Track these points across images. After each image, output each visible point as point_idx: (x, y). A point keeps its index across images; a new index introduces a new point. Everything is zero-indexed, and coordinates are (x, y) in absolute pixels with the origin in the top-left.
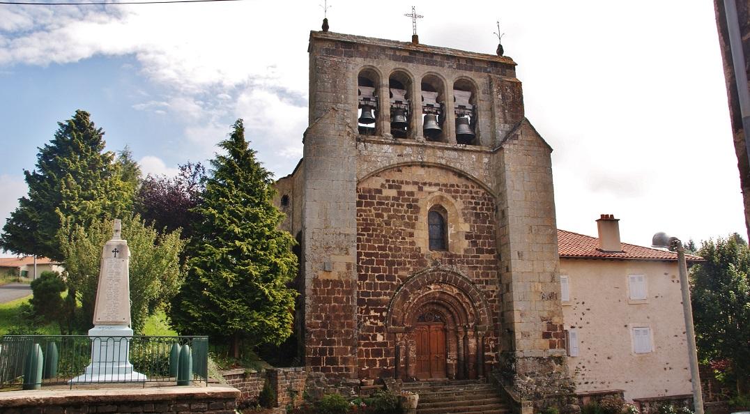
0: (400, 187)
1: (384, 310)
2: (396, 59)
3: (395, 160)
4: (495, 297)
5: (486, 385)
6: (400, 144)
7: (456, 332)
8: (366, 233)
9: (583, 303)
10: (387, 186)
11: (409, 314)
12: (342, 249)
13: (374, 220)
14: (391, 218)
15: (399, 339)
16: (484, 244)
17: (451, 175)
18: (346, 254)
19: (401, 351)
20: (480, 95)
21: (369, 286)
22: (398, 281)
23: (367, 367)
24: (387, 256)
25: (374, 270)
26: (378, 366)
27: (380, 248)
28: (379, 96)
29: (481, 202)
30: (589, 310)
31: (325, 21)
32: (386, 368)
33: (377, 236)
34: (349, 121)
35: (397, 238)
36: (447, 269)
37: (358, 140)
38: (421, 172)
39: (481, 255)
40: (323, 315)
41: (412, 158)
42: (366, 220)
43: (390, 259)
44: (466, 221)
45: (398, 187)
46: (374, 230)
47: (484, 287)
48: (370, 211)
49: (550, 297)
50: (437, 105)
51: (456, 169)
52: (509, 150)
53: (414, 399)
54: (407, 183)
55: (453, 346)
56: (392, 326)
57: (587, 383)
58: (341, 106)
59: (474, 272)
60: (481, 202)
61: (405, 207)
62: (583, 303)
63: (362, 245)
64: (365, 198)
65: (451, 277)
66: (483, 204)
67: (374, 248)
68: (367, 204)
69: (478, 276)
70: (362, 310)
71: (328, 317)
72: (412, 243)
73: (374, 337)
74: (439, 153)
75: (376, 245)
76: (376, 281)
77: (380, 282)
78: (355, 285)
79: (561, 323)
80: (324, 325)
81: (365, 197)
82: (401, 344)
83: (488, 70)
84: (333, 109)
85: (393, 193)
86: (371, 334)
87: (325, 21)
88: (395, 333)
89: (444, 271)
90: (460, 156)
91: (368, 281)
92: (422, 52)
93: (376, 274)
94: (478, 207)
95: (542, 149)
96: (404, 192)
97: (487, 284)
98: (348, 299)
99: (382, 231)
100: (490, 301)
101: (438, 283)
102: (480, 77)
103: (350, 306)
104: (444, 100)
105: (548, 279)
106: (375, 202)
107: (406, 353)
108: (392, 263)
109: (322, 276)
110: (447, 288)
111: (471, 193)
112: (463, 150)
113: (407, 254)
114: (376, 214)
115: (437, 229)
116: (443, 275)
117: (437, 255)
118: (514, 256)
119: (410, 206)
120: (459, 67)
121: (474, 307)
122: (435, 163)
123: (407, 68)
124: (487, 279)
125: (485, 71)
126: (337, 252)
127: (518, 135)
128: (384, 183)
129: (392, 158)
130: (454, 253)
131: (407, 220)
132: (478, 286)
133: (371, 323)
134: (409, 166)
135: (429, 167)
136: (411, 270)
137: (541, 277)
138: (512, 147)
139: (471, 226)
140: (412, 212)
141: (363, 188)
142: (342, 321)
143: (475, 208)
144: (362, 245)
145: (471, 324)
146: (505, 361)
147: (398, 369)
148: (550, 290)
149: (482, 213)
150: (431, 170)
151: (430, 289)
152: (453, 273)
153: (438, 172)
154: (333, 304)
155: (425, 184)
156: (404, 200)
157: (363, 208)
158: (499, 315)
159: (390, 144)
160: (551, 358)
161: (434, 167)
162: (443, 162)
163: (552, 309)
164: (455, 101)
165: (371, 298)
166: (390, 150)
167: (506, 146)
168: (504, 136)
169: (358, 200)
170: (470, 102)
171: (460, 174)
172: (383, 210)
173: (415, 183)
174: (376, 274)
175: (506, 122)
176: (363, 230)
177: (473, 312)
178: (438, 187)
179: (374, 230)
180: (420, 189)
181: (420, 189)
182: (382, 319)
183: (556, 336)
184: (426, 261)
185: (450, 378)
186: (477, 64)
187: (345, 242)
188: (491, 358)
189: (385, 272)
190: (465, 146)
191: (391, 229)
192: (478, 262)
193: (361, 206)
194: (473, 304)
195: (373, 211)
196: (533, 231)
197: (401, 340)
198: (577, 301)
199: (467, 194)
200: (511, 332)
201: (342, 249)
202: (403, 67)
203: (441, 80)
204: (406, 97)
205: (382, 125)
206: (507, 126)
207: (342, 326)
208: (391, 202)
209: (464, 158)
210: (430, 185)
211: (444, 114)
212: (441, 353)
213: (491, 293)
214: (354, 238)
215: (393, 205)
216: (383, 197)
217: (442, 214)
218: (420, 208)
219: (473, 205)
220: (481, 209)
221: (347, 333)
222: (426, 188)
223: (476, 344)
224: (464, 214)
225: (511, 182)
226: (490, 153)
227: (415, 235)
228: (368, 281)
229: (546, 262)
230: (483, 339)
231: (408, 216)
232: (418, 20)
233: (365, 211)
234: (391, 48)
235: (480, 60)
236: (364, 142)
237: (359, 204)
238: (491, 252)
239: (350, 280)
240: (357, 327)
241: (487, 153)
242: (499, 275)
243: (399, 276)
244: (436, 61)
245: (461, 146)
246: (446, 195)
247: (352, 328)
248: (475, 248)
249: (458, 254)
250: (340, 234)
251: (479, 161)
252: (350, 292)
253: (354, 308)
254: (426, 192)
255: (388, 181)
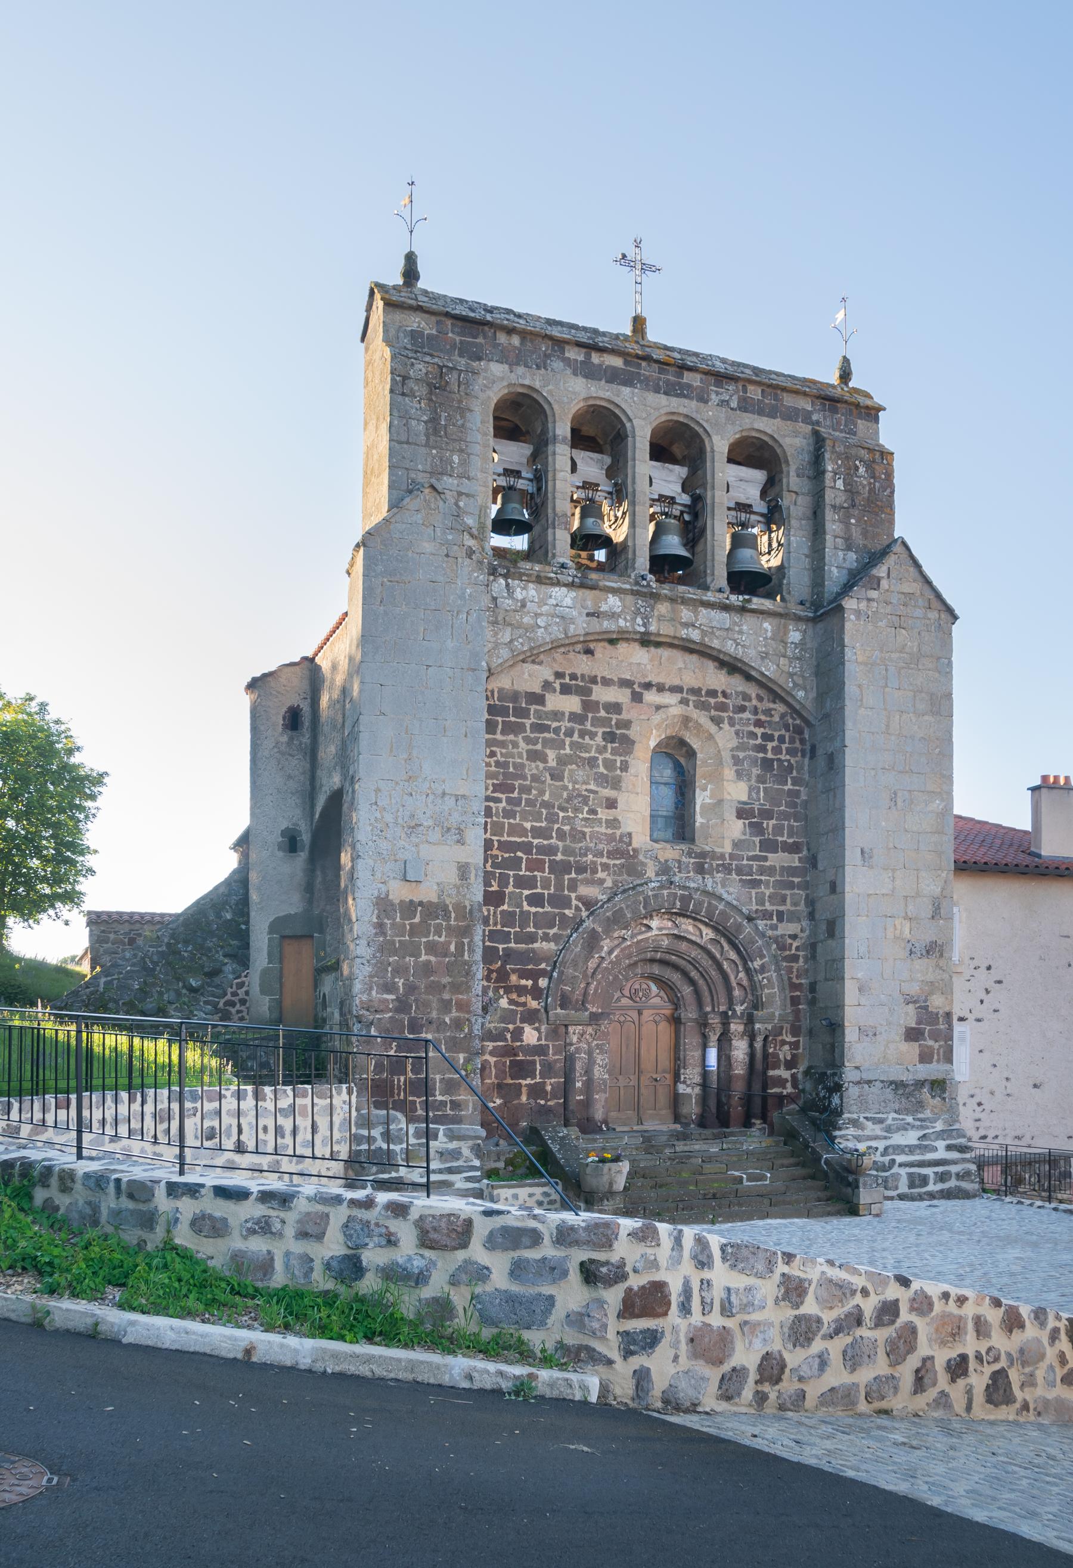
0: (587, 692)
1: (543, 973)
2: (589, 372)
3: (580, 626)
4: (797, 949)
5: (770, 1140)
6: (593, 588)
7: (703, 1024)
8: (503, 796)
9: (989, 968)
10: (557, 686)
11: (599, 983)
12: (449, 829)
13: (523, 766)
14: (565, 764)
15: (575, 1039)
16: (778, 829)
17: (711, 665)
18: (458, 842)
19: (579, 1065)
20: (794, 480)
21: (509, 918)
22: (577, 908)
23: (499, 1101)
24: (551, 850)
25: (521, 883)
26: (524, 1098)
27: (537, 832)
28: (546, 464)
29: (776, 734)
30: (1000, 982)
31: (411, 259)
32: (542, 1102)
33: (529, 802)
34: (470, 521)
35: (576, 810)
36: (692, 885)
37: (493, 572)
38: (640, 656)
39: (770, 855)
40: (400, 982)
41: (622, 623)
42: (505, 765)
43: (559, 857)
44: (739, 775)
45: (584, 692)
46: (525, 790)
47: (774, 928)
48: (515, 745)
49: (928, 952)
50: (685, 499)
51: (725, 654)
52: (858, 613)
53: (620, 1172)
54: (607, 682)
55: (693, 1055)
56: (559, 1010)
57: (984, 1137)
58: (449, 482)
59: (753, 892)
60: (776, 734)
61: (599, 739)
62: (989, 968)
63: (494, 823)
64: (767, 1353)
65: (700, 903)
66: (782, 739)
67: (523, 832)
68: (509, 728)
69: (761, 901)
70: (490, 971)
71: (411, 988)
72: (614, 823)
73: (518, 1034)
74: (686, 614)
75: (528, 825)
76: (526, 907)
77: (533, 910)
78: (477, 914)
79: (947, 1009)
80: (402, 1006)
81: (503, 711)
82: (578, 1050)
83: (815, 417)
84: (432, 487)
85: (572, 704)
86: (511, 1027)
87: (411, 259)
88: (566, 1026)
89: (685, 888)
90: (736, 623)
91: (505, 907)
92: (657, 362)
93: (526, 892)
94: (770, 746)
95: (933, 615)
96: (597, 703)
97: (780, 919)
98: (460, 947)
99: (542, 793)
100: (785, 959)
101: (671, 914)
102: (796, 434)
103: (466, 963)
104: (704, 485)
105: (927, 911)
106: (528, 723)
107: (588, 1072)
108: (565, 867)
109: (399, 892)
110: (687, 927)
111: (755, 711)
112: (743, 610)
113: (601, 846)
114: (528, 751)
115: (668, 795)
116: (682, 897)
117: (670, 853)
118: (852, 856)
119: (610, 737)
120: (745, 406)
121: (748, 971)
122: (675, 637)
123: (617, 400)
124: (781, 908)
125: (807, 418)
126: (435, 835)
127: (879, 579)
128: (551, 678)
129: (572, 621)
130: (708, 848)
131: (602, 769)
132: (761, 924)
133: (511, 1002)
134: (612, 642)
135: (658, 645)
136: (609, 883)
137: (910, 907)
138: (863, 605)
139: (751, 789)
140: (614, 752)
141: (500, 690)
142: (446, 996)
143: (762, 749)
144: (494, 823)
145: (739, 1009)
146: (816, 1088)
147: (572, 1106)
148: (928, 934)
149: (779, 760)
150: (665, 653)
151: (649, 928)
152: (706, 893)
153: (680, 659)
154: (424, 958)
155: (648, 686)
156: (597, 722)
157: (499, 737)
158: (806, 987)
159: (571, 585)
160: (920, 1084)
161: (671, 646)
162: (695, 635)
163: (930, 977)
164: (728, 491)
165: (512, 945)
166: (568, 601)
167: (849, 604)
168: (844, 579)
169: (486, 716)
170: (764, 493)
171: (732, 666)
172: (546, 743)
173: (625, 683)
174: (526, 892)
175: (849, 548)
176: (497, 788)
177: (745, 983)
178: (679, 696)
179: (525, 790)
180: (637, 698)
181: (637, 698)
182: (536, 992)
183: (935, 1036)
184: (644, 864)
185: (686, 1125)
186: (789, 400)
187: (456, 815)
188: (781, 1082)
189: (546, 886)
190: (749, 601)
191: (565, 788)
192: (762, 871)
193: (494, 733)
194: (745, 964)
195: (522, 744)
196: (899, 803)
197: (579, 1040)
198: (976, 963)
199: (746, 715)
200: (835, 1027)
201: (449, 829)
202: (607, 395)
203: (697, 435)
204: (611, 472)
205: (550, 538)
206: (852, 556)
207: (446, 1006)
208: (565, 724)
209: (745, 628)
210: (661, 688)
211: (699, 524)
212: (664, 1071)
213: (789, 941)
214: (479, 806)
215: (569, 733)
216: (546, 713)
217: (682, 760)
218: (633, 742)
219: (759, 741)
220: (777, 750)
221: (458, 1024)
222: (651, 697)
223: (747, 1050)
224: (737, 761)
225: (857, 691)
226: (808, 620)
227: (621, 805)
228: (505, 907)
229: (923, 874)
230: (766, 1039)
231: (605, 760)
232: (649, 278)
233: (502, 744)
234: (579, 345)
235: (797, 392)
236: (506, 576)
237: (491, 727)
238: (793, 848)
239: (467, 903)
240: (480, 1012)
241: (798, 619)
242: (811, 902)
243: (578, 898)
244: (689, 386)
245: (735, 599)
246: (695, 714)
247: (469, 1012)
248: (757, 840)
249: (718, 850)
250: (444, 794)
251: (780, 637)
252: (466, 931)
253: (474, 968)
254: (649, 705)
255: (559, 675)
